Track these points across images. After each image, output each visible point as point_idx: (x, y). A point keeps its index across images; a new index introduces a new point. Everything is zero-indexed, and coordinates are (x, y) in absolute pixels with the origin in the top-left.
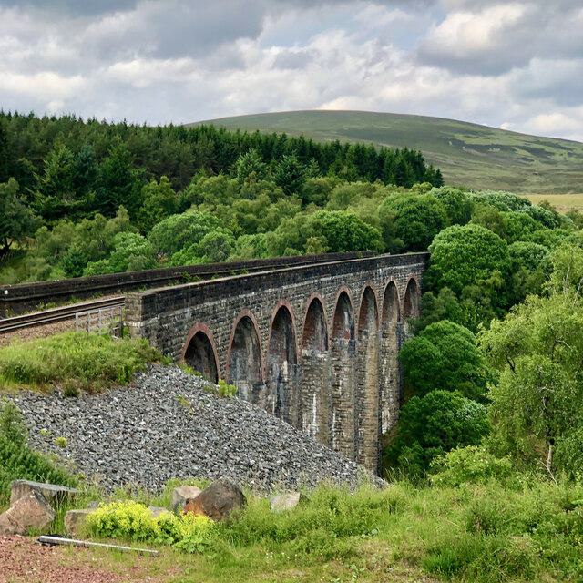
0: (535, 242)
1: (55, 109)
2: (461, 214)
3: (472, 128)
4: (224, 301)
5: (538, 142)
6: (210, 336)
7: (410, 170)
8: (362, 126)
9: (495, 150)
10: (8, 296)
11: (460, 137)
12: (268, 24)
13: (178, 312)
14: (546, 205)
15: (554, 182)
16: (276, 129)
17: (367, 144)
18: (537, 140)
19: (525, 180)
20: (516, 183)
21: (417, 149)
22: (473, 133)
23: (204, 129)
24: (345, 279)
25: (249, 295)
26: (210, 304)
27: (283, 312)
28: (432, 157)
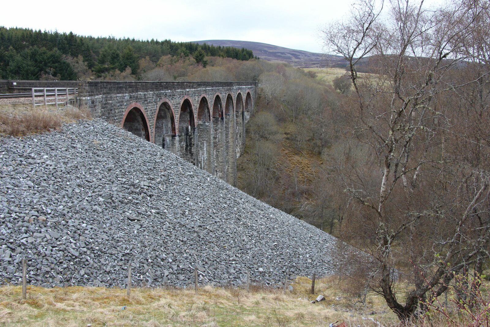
9: (279, 54)
11: (266, 49)
18: (294, 51)
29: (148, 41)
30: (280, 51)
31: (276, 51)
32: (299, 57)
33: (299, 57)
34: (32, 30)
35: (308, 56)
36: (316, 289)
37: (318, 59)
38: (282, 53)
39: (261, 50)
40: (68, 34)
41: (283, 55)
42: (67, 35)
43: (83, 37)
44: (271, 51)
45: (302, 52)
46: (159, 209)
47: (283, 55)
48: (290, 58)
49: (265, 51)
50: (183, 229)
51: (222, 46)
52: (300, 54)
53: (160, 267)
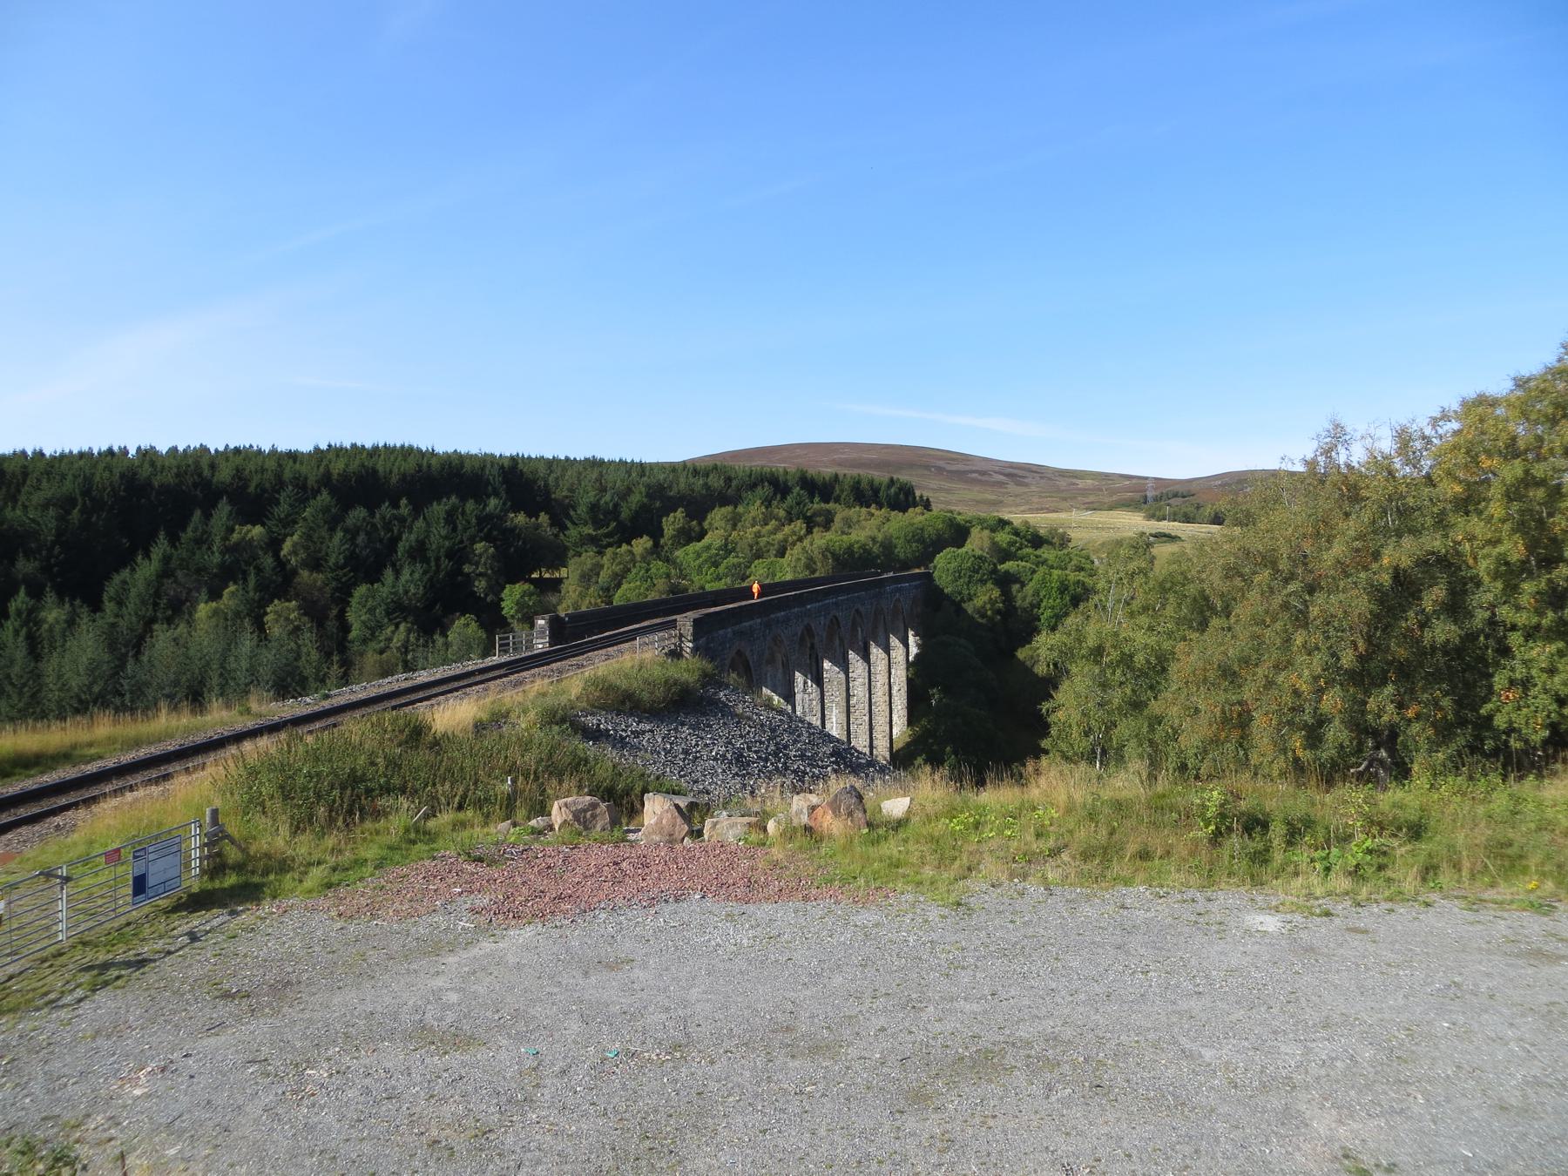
0: (1460, 870)
1: (22, 731)
2: (958, 533)
3: (954, 456)
4: (759, 621)
5: (1012, 467)
6: (748, 653)
7: (903, 499)
8: (854, 455)
9: (974, 475)
10: (568, 622)
11: (941, 463)
12: (503, 596)
13: (721, 632)
14: (1026, 523)
15: (1027, 503)
16: (779, 466)
17: (862, 472)
18: (1012, 465)
19: (1001, 502)
20: (996, 504)
21: (903, 477)
22: (953, 460)
23: (715, 467)
24: (858, 597)
25: (779, 615)
26: (747, 624)
27: (808, 630)
28: (925, 487)
29: (395, 446)
30: (974, 468)
31: (967, 468)
32: (1026, 480)
33: (1026, 480)
34: (24, 453)
35: (1049, 479)
36: (1316, 815)
37: (1074, 484)
38: (983, 473)
39: (927, 467)
40: (164, 452)
41: (984, 478)
42: (322, 451)
43: (378, 447)
44: (954, 468)
45: (1034, 469)
46: (33, 1094)
47: (984, 478)
48: (1001, 484)
49: (940, 470)
50: (904, 999)
51: (718, 463)
52: (1028, 474)
53: (13, 1139)
